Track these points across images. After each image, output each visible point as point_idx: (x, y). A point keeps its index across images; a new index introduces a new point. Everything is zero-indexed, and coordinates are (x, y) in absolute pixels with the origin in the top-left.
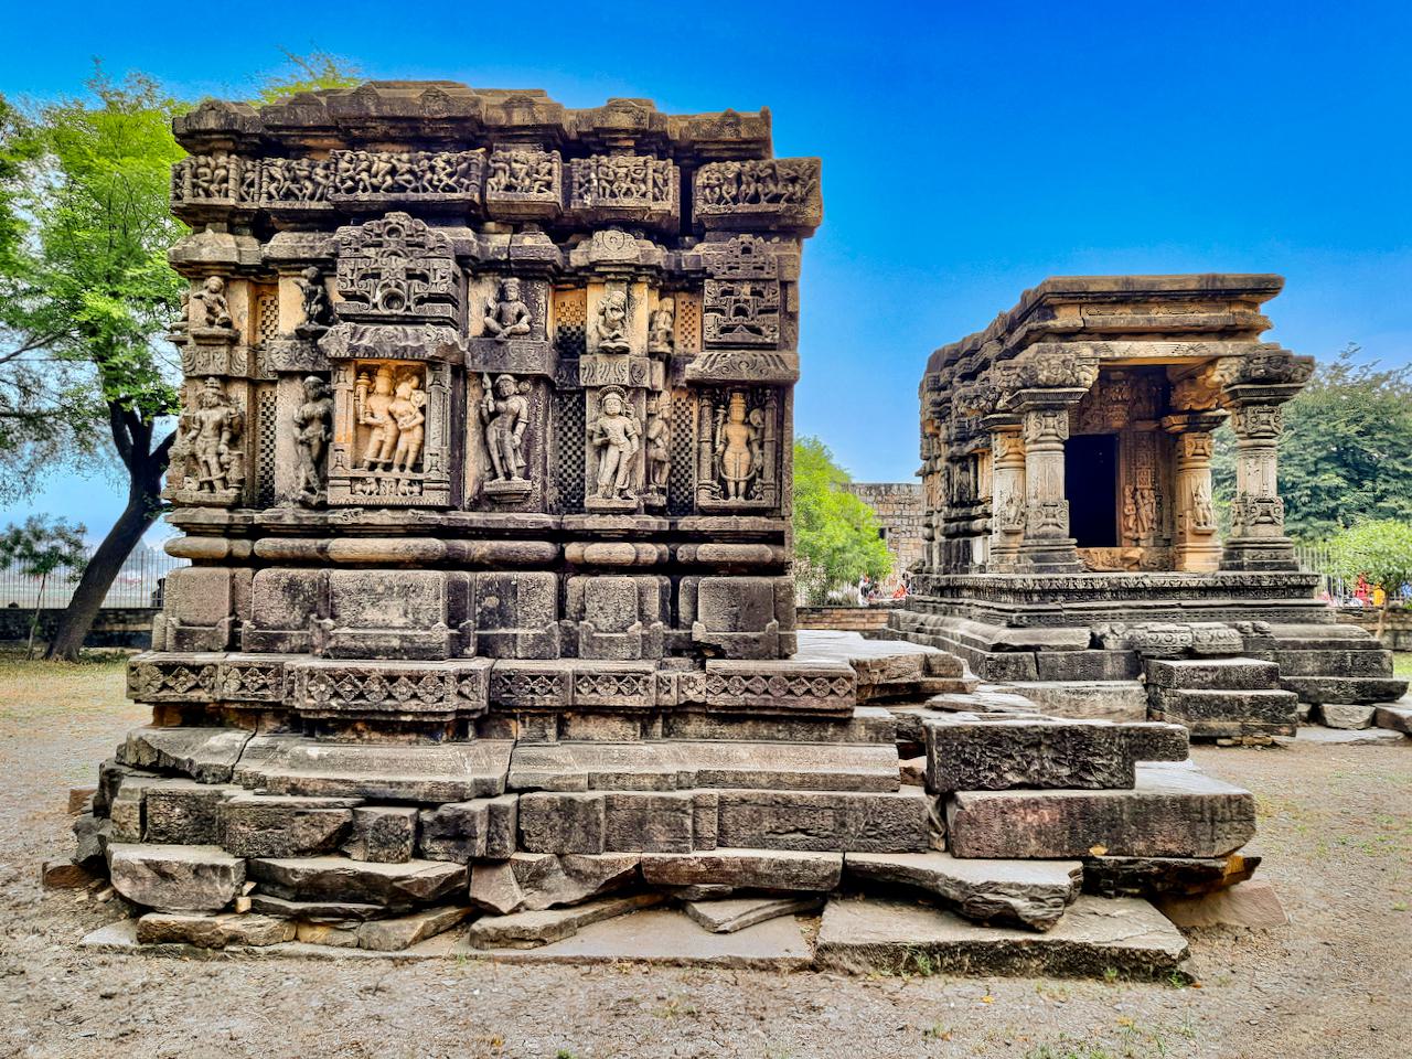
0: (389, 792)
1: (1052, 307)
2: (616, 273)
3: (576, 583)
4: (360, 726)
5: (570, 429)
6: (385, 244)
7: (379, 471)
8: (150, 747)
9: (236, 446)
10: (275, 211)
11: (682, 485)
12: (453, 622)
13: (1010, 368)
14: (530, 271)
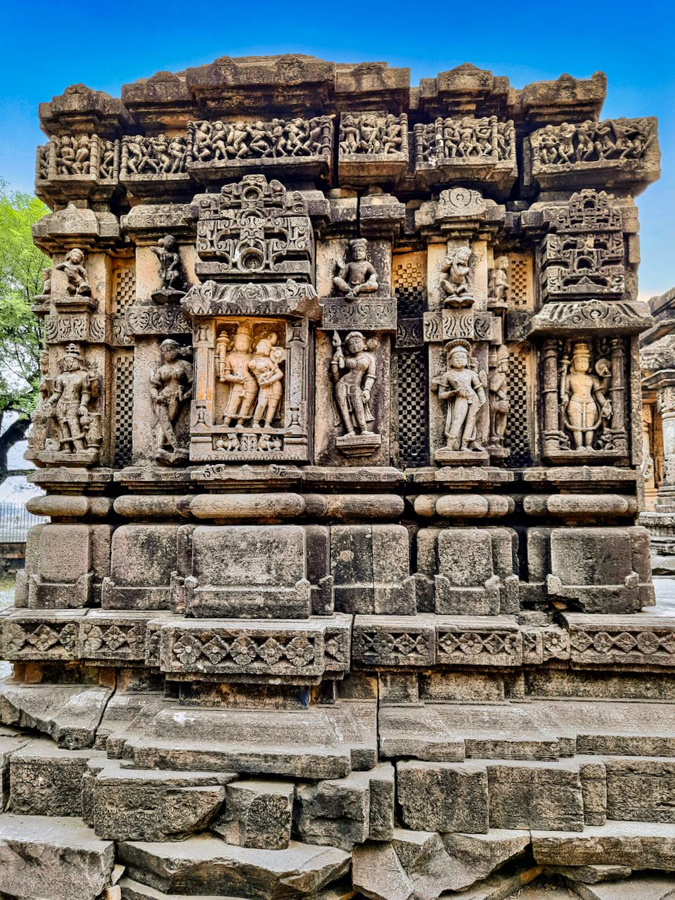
0: (264, 767)
2: (460, 231)
3: (426, 534)
4: (225, 689)
5: (409, 385)
6: (244, 206)
7: (239, 427)
8: (11, 706)
9: (94, 408)
10: (134, 184)
11: (518, 437)
12: (312, 577)
14: (376, 230)
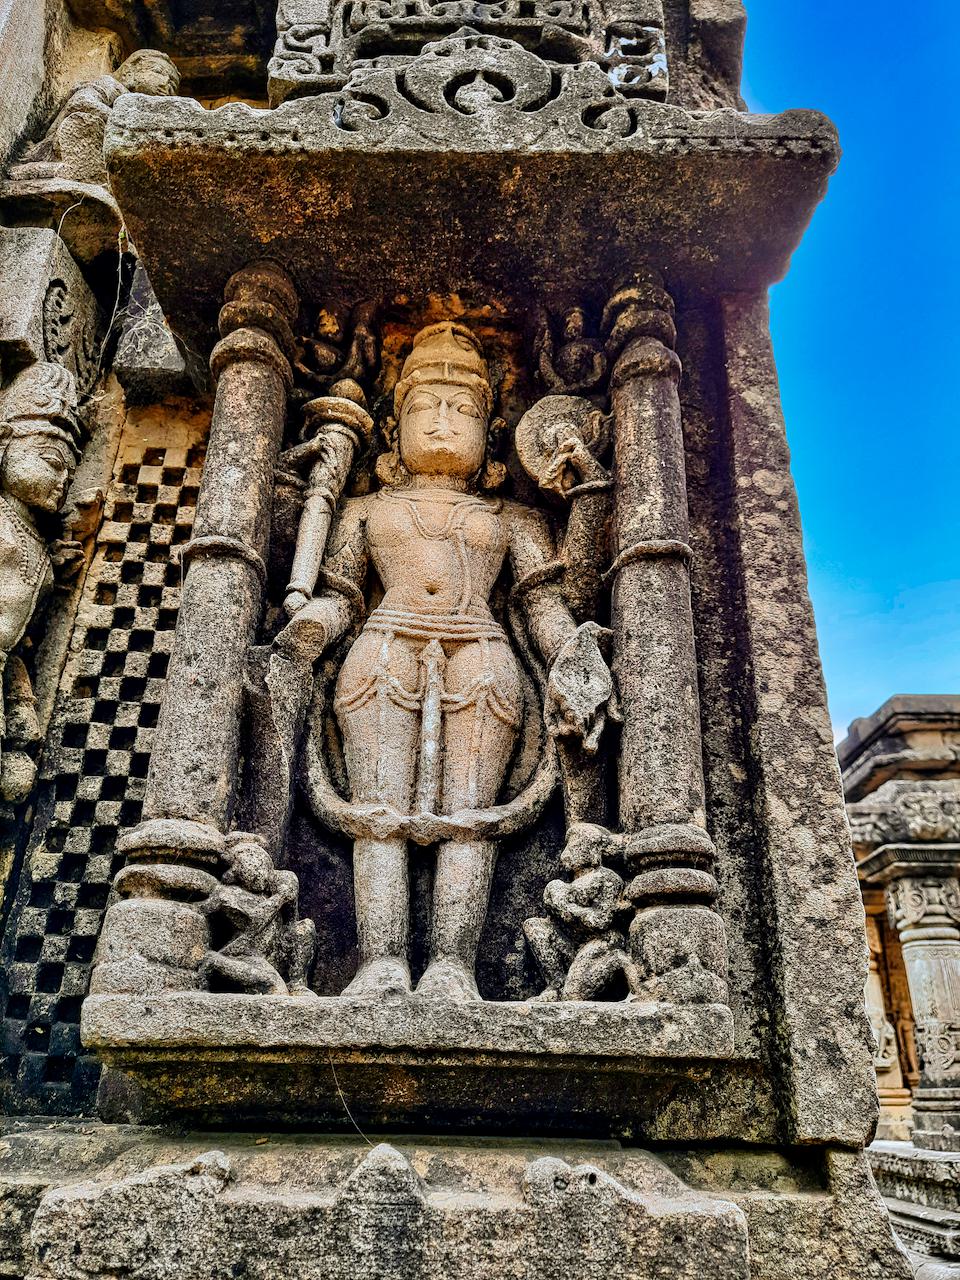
1: (901, 735)
13: (860, 815)
